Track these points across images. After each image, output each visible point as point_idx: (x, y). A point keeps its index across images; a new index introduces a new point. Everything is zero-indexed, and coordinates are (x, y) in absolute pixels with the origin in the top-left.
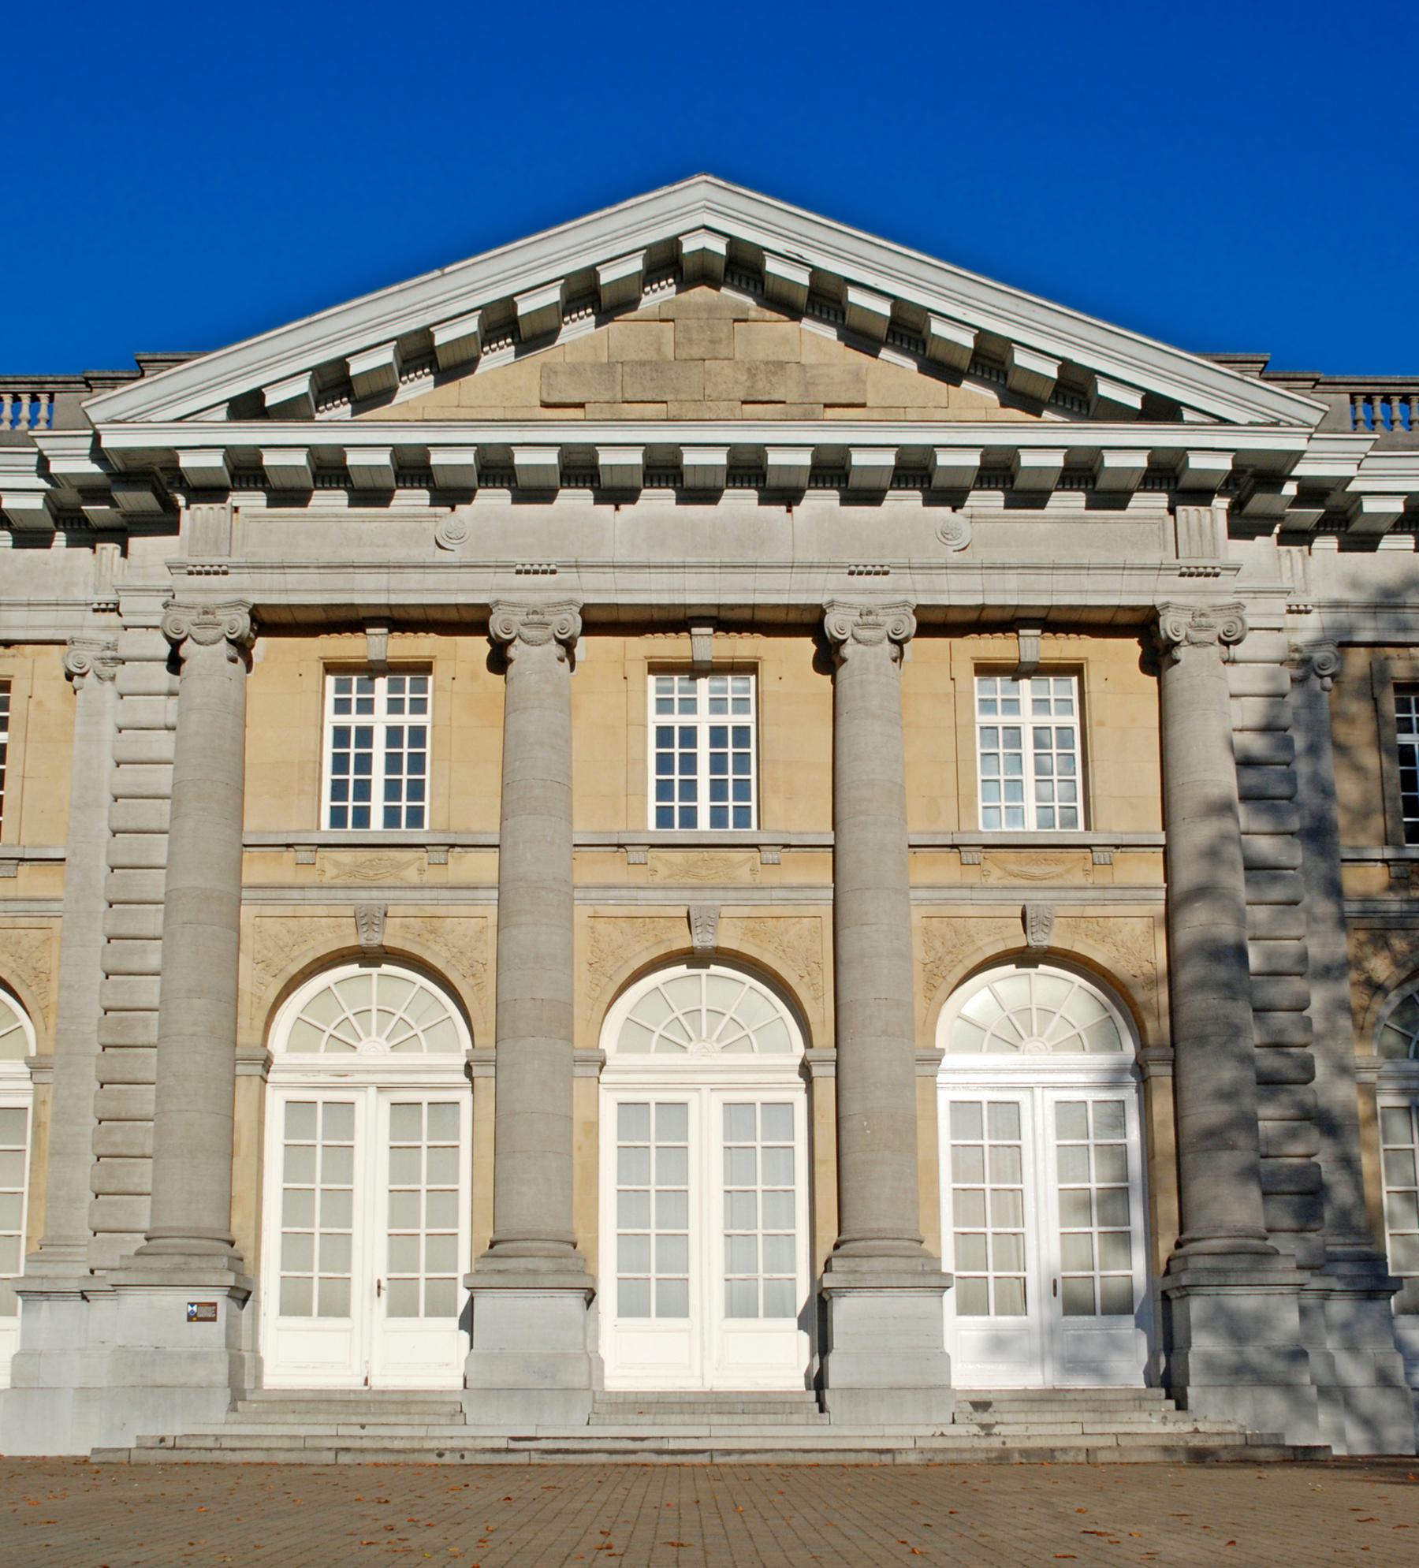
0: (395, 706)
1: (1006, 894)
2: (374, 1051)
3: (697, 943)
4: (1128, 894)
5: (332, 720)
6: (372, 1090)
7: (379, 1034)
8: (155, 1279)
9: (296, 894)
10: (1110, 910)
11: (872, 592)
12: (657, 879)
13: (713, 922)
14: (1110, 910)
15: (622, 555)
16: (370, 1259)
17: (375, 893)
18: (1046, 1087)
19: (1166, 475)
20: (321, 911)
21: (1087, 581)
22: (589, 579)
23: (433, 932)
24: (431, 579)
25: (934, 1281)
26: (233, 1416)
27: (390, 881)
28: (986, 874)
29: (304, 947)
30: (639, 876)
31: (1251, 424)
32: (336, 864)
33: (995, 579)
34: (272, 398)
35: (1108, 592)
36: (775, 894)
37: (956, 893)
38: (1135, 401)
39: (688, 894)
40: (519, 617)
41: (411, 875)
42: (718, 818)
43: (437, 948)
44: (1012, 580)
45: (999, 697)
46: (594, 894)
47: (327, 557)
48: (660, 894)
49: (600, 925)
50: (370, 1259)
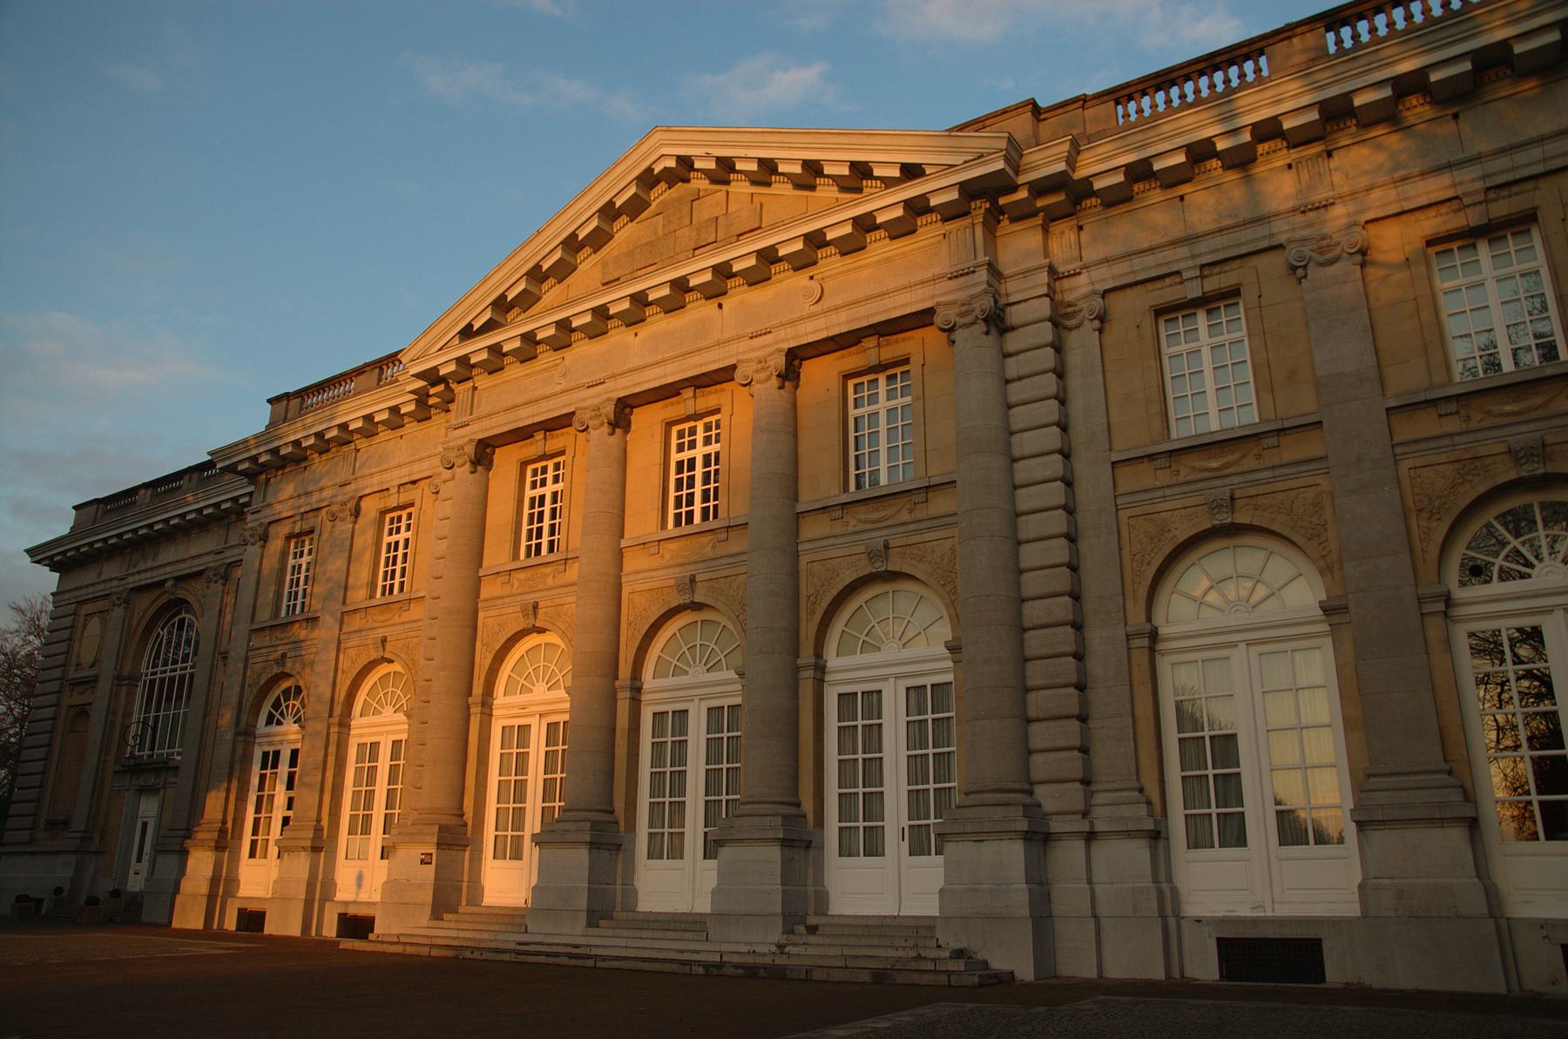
1: (857, 537)
4: (936, 523)
6: (1242, 646)
7: (1532, 566)
9: (500, 602)
10: (926, 537)
14: (926, 537)
16: (896, 815)
18: (898, 677)
21: (888, 303)
26: (592, 931)
35: (903, 306)
36: (724, 561)
37: (826, 542)
38: (896, 173)
49: (1132, 522)
50: (896, 815)
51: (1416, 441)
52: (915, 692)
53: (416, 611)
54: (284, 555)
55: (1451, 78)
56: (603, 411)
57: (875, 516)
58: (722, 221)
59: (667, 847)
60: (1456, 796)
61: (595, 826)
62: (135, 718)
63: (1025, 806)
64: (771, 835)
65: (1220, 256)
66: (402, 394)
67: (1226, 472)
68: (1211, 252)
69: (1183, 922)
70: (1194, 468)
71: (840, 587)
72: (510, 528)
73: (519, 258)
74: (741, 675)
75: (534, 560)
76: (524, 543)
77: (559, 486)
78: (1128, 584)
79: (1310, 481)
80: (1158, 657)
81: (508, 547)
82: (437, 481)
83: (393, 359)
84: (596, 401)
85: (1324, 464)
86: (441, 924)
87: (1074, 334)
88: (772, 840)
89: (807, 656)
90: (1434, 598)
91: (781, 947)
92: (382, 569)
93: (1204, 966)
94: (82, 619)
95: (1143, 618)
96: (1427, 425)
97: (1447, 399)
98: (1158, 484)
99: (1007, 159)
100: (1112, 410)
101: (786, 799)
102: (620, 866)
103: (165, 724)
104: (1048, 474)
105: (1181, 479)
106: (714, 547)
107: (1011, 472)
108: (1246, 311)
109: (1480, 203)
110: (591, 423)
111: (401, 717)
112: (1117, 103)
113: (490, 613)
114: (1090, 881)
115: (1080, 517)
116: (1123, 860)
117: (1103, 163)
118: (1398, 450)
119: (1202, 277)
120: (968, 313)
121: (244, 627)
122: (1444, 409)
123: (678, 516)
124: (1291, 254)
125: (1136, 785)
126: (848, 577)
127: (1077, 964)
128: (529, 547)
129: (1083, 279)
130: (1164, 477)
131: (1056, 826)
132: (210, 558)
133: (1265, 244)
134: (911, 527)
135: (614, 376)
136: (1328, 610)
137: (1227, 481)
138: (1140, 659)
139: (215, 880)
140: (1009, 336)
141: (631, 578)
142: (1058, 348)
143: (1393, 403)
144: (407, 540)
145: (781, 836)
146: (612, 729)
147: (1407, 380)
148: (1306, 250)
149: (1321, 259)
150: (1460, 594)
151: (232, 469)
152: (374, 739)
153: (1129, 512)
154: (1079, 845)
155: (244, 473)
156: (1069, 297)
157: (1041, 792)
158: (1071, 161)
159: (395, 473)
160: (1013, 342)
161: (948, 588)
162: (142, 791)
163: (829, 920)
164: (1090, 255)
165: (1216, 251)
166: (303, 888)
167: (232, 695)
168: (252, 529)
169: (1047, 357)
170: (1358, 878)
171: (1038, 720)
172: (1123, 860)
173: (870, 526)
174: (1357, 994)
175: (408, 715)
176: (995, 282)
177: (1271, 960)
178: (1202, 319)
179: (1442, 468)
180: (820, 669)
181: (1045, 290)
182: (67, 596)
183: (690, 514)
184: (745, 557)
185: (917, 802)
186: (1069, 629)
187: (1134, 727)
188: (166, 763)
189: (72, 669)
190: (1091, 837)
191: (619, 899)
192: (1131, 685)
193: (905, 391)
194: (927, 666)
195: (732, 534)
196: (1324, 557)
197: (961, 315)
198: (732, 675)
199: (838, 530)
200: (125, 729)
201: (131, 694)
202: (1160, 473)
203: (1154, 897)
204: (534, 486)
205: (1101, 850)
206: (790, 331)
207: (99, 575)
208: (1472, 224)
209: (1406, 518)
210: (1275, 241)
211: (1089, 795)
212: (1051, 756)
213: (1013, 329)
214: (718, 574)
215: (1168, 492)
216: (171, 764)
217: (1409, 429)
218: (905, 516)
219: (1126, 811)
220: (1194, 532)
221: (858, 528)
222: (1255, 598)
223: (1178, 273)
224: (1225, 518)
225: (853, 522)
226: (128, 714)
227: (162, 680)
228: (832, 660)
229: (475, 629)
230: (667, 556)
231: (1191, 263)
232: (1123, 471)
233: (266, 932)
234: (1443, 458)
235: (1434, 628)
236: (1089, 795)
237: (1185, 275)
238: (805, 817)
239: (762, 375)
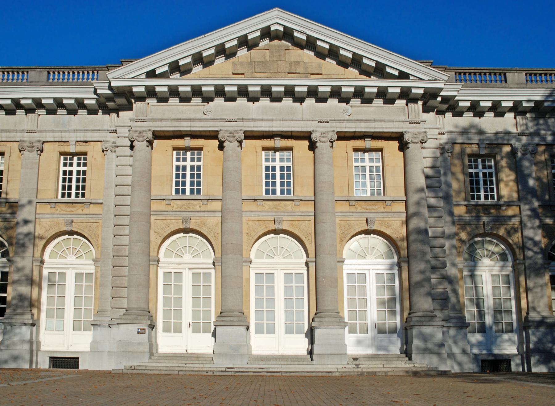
3: (276, 228)
4: (395, 214)
5: (175, 164)
6: (187, 269)
8: (128, 322)
9: (166, 213)
12: (266, 209)
13: (281, 222)
14: (391, 219)
15: (255, 117)
16: (187, 317)
17: (187, 213)
18: (73, 268)
19: (405, 94)
20: (173, 218)
22: (247, 123)
23: (204, 224)
24: (202, 123)
25: (343, 324)
26: (150, 360)
27: (192, 210)
29: (168, 228)
30: (260, 209)
31: (429, 80)
32: (177, 205)
33: (358, 124)
34: (158, 72)
35: (299, 127)
39: (274, 214)
40: (227, 134)
41: (197, 208)
42: (282, 192)
43: (205, 229)
44: (363, 124)
45: (360, 158)
46: (248, 214)
47: (174, 117)
48: (266, 214)
49: (250, 222)
50: (187, 317)
134: (385, 214)
194: (201, 266)
214: (295, 219)
224: (69, 228)
233: (81, 368)
237: (71, 143)
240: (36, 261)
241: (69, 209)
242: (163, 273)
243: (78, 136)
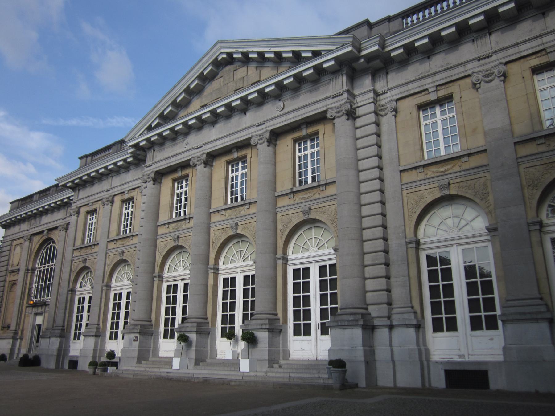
0: (312, 147)
2: (313, 251)
11: (262, 129)
16: (315, 319)
18: (317, 262)
19: (319, 70)
26: (139, 365)
27: (180, 229)
28: (549, 145)
31: (337, 48)
34: (153, 125)
38: (310, 55)
51: (527, 156)
52: (322, 269)
53: (135, 240)
54: (86, 219)
55: (450, 34)
56: (202, 158)
57: (306, 196)
58: (245, 79)
59: (114, 336)
60: (543, 309)
61: (199, 324)
62: (34, 285)
63: (363, 315)
64: (264, 327)
65: (444, 81)
66: (127, 155)
67: (446, 173)
68: (532, 48)
69: (431, 364)
70: (433, 172)
71: (292, 226)
72: (168, 206)
73: (168, 97)
74: (336, 250)
75: (235, 204)
76: (174, 212)
77: (187, 189)
78: (407, 221)
79: (482, 175)
80: (420, 252)
81: (222, 199)
82: (142, 188)
83: (122, 142)
84: (199, 154)
85: (487, 168)
86: (140, 365)
87: (385, 118)
88: (265, 329)
89: (280, 253)
90: (535, 223)
91: (266, 373)
92: (123, 224)
93: (439, 381)
94: (13, 247)
95: (413, 235)
96: (531, 149)
97: (540, 137)
98: (419, 179)
99: (353, 46)
100: (400, 149)
101: (271, 312)
102: (209, 340)
103: (45, 288)
104: (373, 176)
105: (428, 176)
106: (245, 211)
107: (358, 176)
108: (455, 104)
109: (434, 91)
110: (197, 163)
111: (129, 282)
112: (403, 19)
113: (162, 240)
114: (391, 345)
115: (386, 193)
116: (404, 337)
117: (395, 47)
118: (519, 160)
119: (437, 90)
120: (261, 139)
121: (69, 249)
122: (539, 142)
123: (232, 199)
124: (474, 79)
125: (410, 305)
126: (295, 222)
127: (384, 379)
128: (176, 213)
129: (388, 94)
130: (422, 176)
131: (376, 322)
132: (61, 221)
133: (463, 75)
134: (319, 201)
135: (206, 144)
136: (491, 230)
137: (447, 177)
138: (412, 252)
139: (59, 350)
140: (358, 120)
141: (214, 224)
142: (378, 124)
143: (517, 140)
144: (132, 212)
145: (267, 327)
146: (207, 286)
147: (521, 129)
148: (480, 76)
149: (486, 79)
150: (546, 221)
151: (65, 186)
152: (120, 292)
153: (524, 166)
154: (386, 331)
155: (69, 187)
156: (382, 103)
157: (370, 308)
158: (383, 45)
159: (126, 186)
160: (359, 122)
161: (334, 225)
162: (37, 314)
163: (158, 359)
164: (390, 86)
165: (443, 79)
166: (92, 352)
167: (65, 276)
168: (73, 209)
169: (372, 128)
170: (503, 344)
171: (370, 278)
172: (404, 337)
173: (304, 201)
174: (500, 393)
175: (132, 282)
176: (351, 99)
177: (466, 378)
178: (438, 110)
179: (538, 167)
180: (285, 259)
181: (372, 100)
182: (8, 238)
183: (236, 198)
184: (191, 229)
185: (324, 313)
186: (381, 241)
187: (409, 281)
188: (45, 303)
189: (10, 266)
190: (391, 327)
191: (209, 354)
192: (408, 263)
193: (318, 145)
195: (252, 206)
196: (488, 207)
197: (337, 112)
198: (332, 251)
199: (292, 202)
200: (30, 289)
201: (32, 277)
202: (419, 174)
203: (417, 352)
204: (178, 189)
205: (396, 333)
206: (271, 123)
207: (20, 229)
208: (551, 60)
209: (522, 189)
210: (467, 73)
211: (390, 310)
212: (375, 293)
213: (359, 117)
215: (423, 182)
216: (47, 303)
217: (524, 150)
218: (317, 196)
219: (406, 316)
220: (434, 198)
221: (299, 202)
222: (461, 226)
223: (427, 90)
225: (297, 199)
226: (31, 284)
227: (44, 270)
228: (221, 266)
229: (156, 247)
230: (171, 229)
231: (432, 85)
232: (404, 175)
234: (539, 163)
235: (535, 237)
236: (390, 310)
237: (430, 90)
238: (279, 319)
239: (261, 141)
240: (104, 286)
241: (442, 170)
242: (461, 251)
243: (410, 88)
